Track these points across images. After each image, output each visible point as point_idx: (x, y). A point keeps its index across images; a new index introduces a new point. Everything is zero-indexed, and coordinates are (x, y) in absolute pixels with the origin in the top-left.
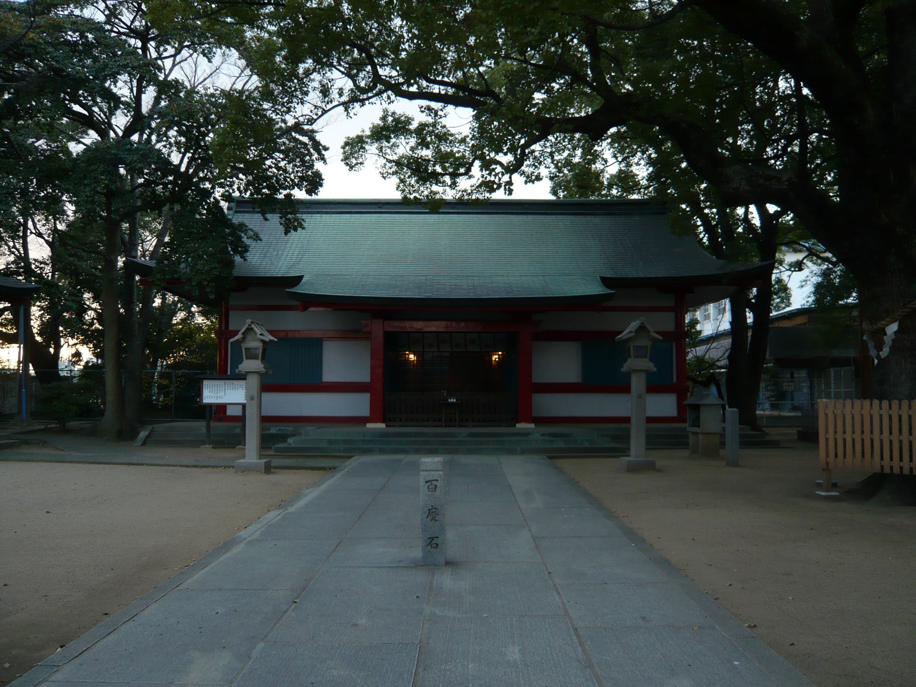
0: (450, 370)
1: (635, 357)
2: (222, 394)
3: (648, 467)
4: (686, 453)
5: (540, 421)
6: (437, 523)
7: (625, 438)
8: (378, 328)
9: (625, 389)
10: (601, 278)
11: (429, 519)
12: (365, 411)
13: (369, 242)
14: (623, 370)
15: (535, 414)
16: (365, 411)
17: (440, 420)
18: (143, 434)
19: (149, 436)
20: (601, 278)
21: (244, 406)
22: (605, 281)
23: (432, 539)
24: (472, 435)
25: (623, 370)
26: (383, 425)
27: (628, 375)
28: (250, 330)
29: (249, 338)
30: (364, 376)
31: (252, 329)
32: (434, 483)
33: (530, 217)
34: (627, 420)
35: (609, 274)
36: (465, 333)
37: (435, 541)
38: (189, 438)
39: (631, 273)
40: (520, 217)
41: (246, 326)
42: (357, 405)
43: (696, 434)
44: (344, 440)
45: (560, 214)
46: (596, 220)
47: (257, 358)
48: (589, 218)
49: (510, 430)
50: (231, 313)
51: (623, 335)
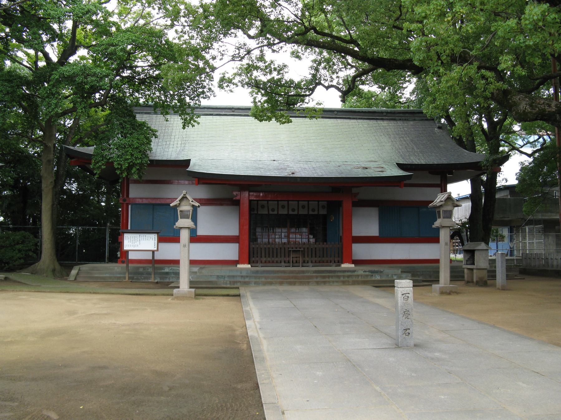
0: (295, 226)
1: (444, 218)
2: (138, 243)
3: (504, 289)
4: (463, 283)
5: (357, 262)
6: (409, 320)
7: (436, 273)
8: (245, 197)
9: (436, 240)
10: (397, 164)
11: (404, 318)
12: (235, 257)
13: (230, 136)
14: (433, 226)
15: (355, 257)
16: (235, 257)
17: (289, 262)
18: (74, 272)
19: (78, 274)
20: (397, 164)
21: (153, 252)
22: (401, 166)
23: (406, 330)
24: (316, 272)
25: (433, 226)
26: (249, 266)
27: (438, 230)
28: (184, 198)
29: (183, 203)
30: (233, 230)
31: (186, 197)
32: (407, 295)
33: (339, 120)
34: (437, 261)
35: (401, 162)
36: (258, 201)
37: (408, 331)
38: (108, 275)
39: (415, 160)
40: (332, 120)
41: (182, 195)
42: (230, 252)
43: (472, 270)
44: (228, 276)
45: (359, 119)
46: (392, 124)
47: (188, 218)
48: (380, 122)
49: (337, 268)
50: (131, 186)
51: (434, 204)
